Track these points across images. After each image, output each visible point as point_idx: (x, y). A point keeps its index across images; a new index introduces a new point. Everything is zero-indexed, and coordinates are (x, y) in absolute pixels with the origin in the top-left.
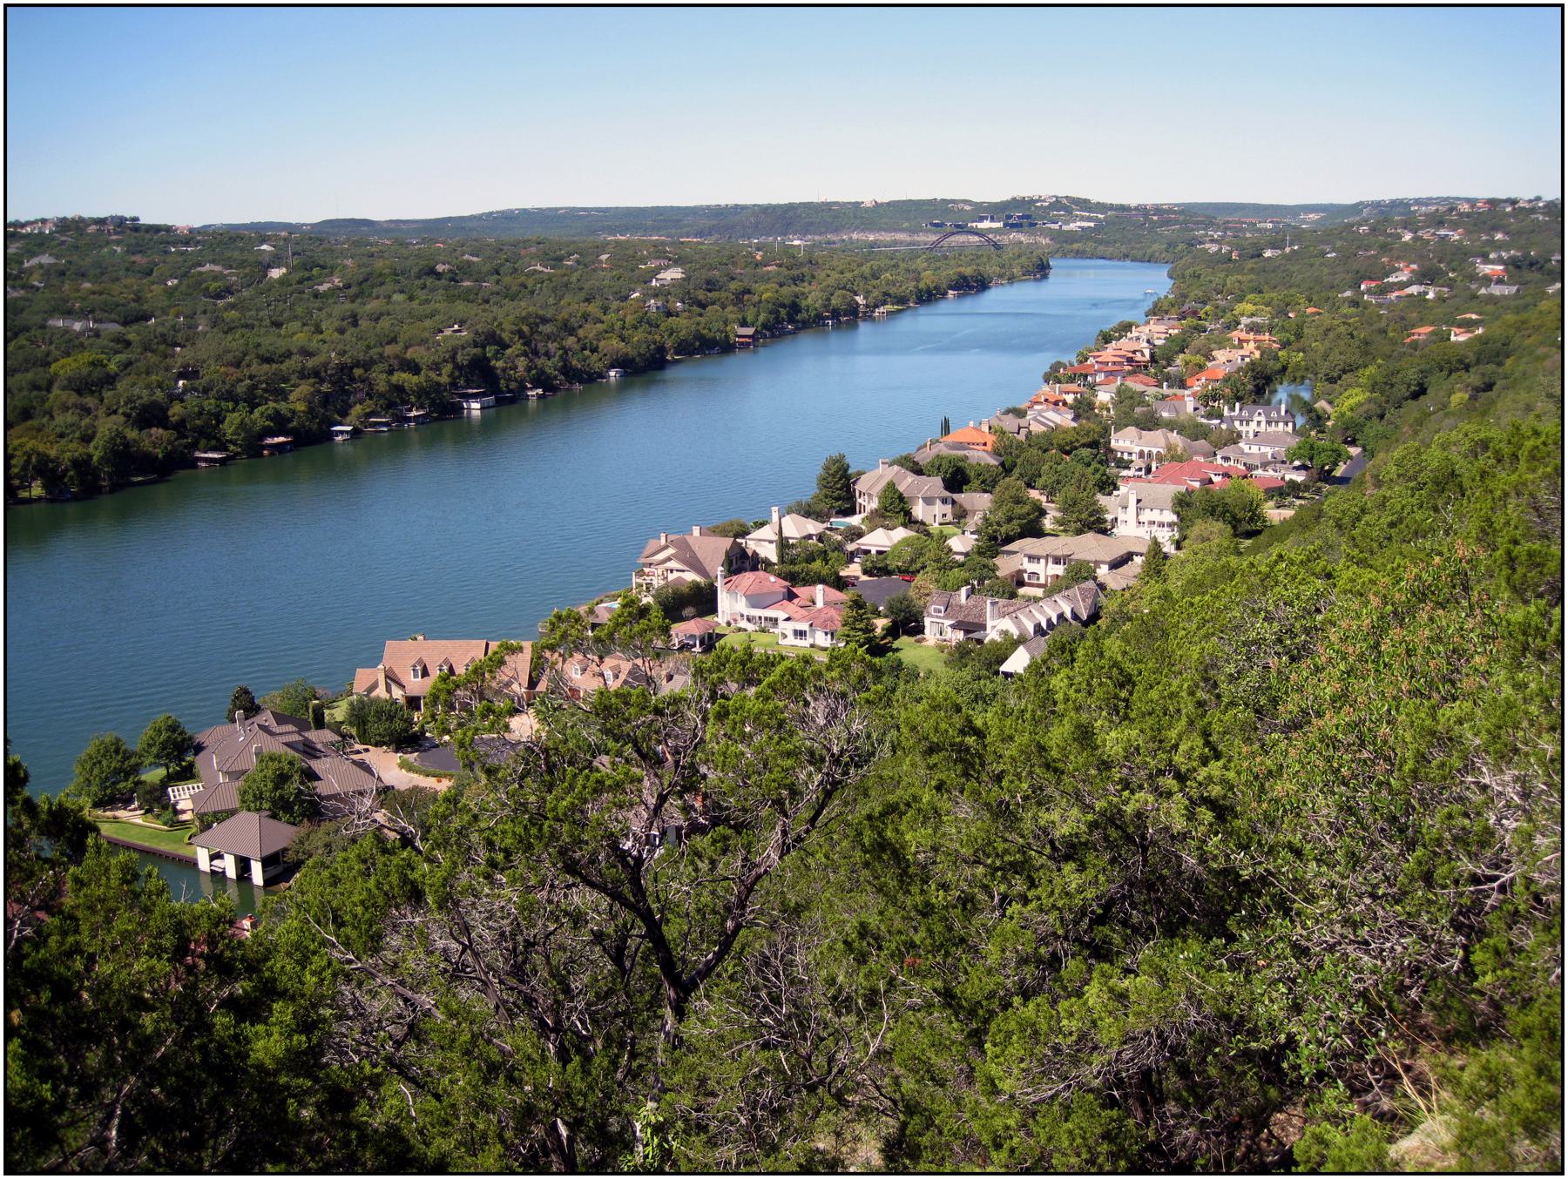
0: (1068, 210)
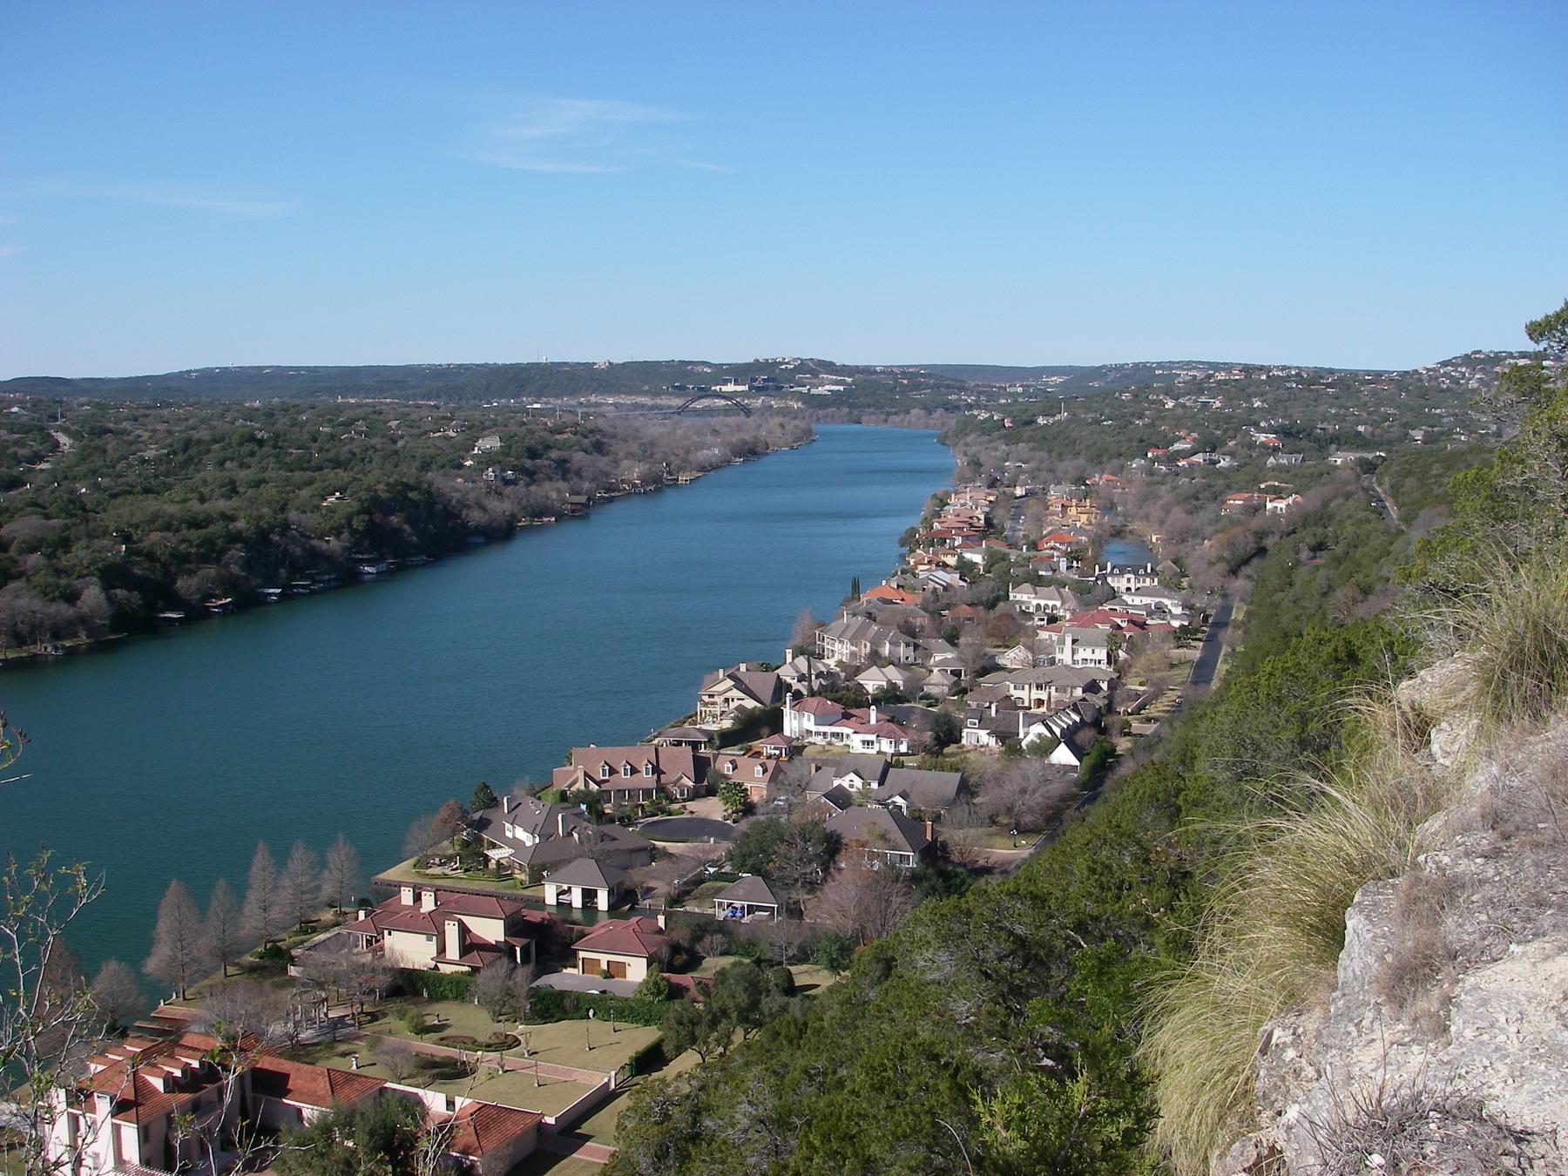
0: (815, 374)
